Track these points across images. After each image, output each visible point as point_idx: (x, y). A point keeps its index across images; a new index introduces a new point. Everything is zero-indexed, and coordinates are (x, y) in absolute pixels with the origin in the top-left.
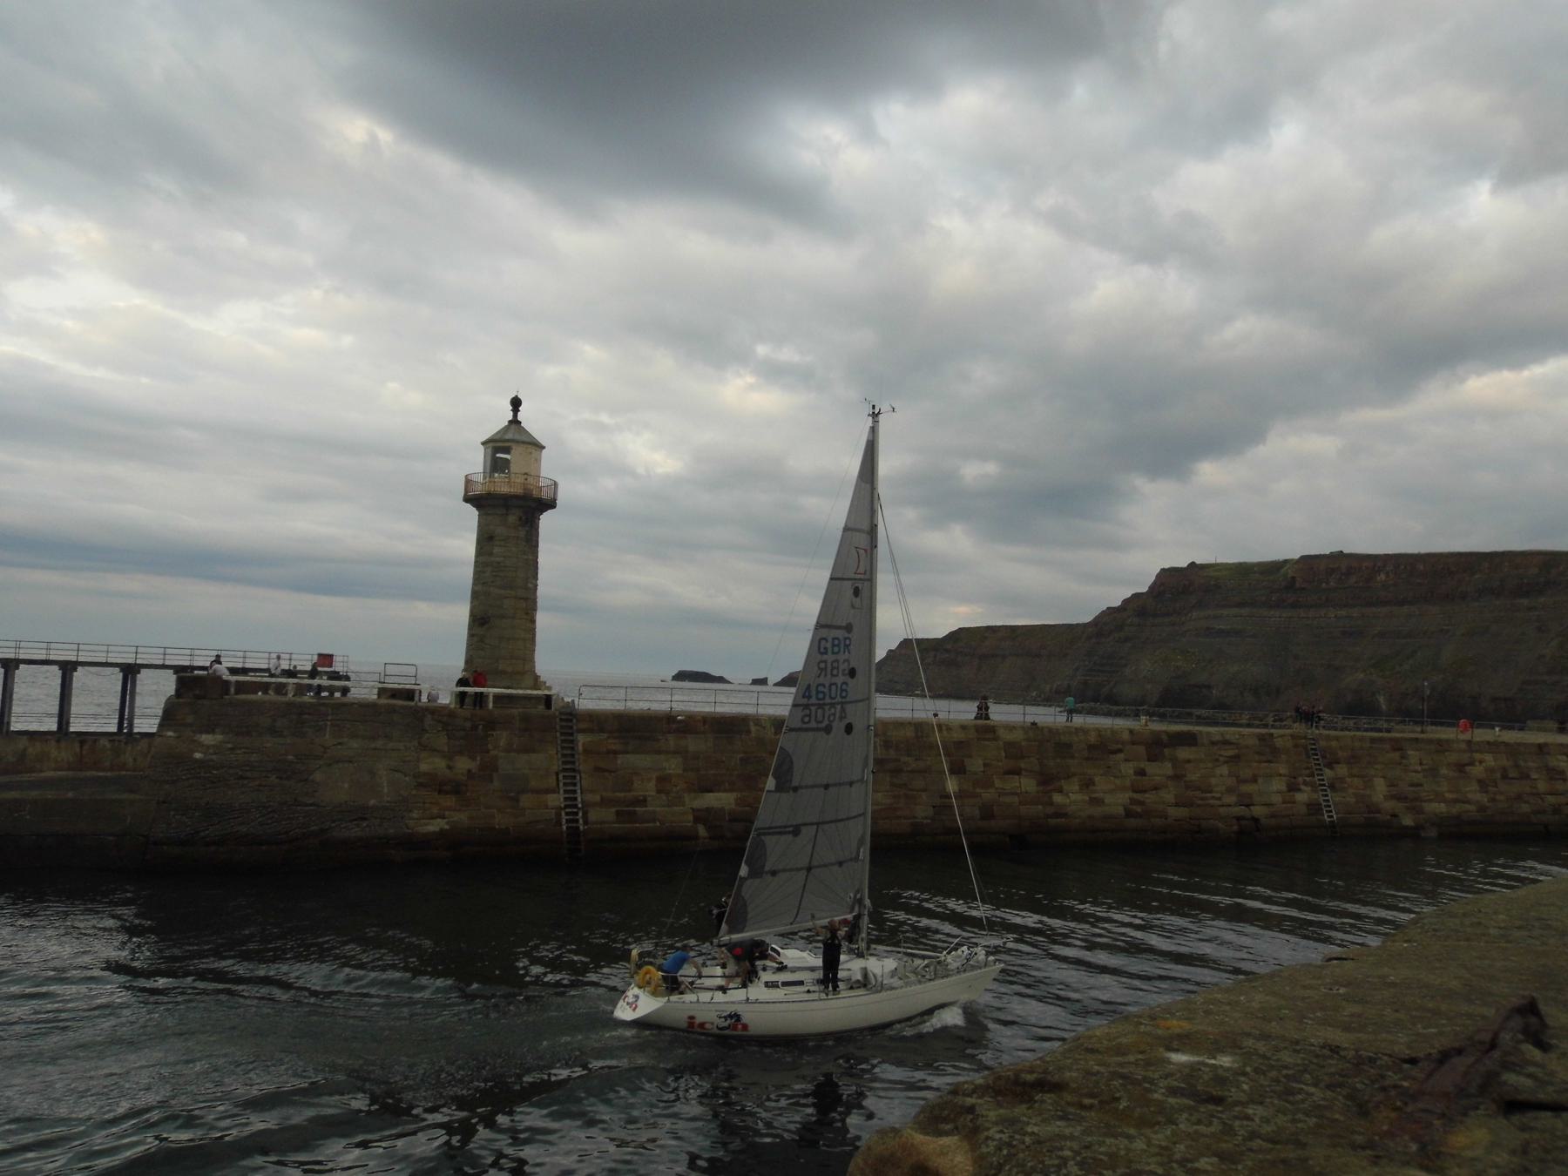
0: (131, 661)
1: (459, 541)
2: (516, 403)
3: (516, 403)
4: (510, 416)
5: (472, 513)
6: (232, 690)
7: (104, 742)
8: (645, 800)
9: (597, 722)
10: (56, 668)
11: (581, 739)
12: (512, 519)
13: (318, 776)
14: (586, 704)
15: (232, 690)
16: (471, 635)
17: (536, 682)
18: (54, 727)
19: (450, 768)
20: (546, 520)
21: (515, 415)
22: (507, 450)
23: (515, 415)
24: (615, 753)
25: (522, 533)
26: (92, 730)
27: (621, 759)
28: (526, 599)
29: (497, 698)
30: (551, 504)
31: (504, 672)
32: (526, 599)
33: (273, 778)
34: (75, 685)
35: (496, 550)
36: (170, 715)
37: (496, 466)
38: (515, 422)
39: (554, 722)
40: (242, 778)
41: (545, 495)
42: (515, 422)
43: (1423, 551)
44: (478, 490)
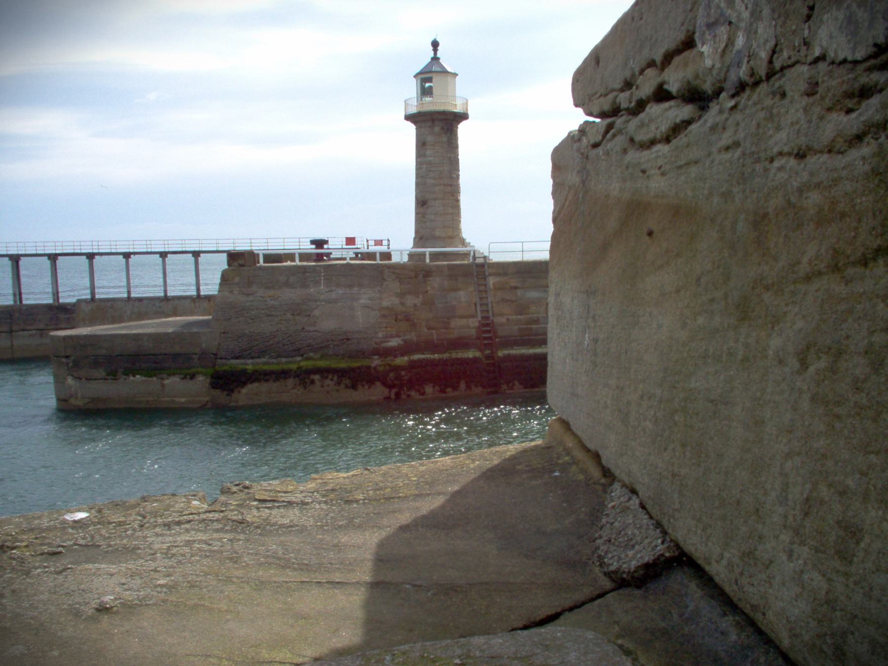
0: (91, 251)
1: (402, 145)
2: (435, 45)
3: (435, 45)
4: (432, 54)
5: (411, 129)
6: (261, 260)
7: (83, 304)
8: (538, 320)
9: (504, 269)
10: (84, 257)
11: (491, 281)
12: (437, 129)
13: (317, 313)
14: (495, 258)
15: (261, 260)
16: (417, 214)
17: (463, 242)
18: (89, 297)
19: (402, 304)
20: (463, 129)
21: (435, 53)
22: (430, 80)
23: (435, 53)
24: (516, 288)
25: (445, 139)
26: (111, 296)
27: (519, 293)
28: (451, 185)
29: (431, 254)
30: (464, 116)
31: (439, 238)
32: (451, 185)
33: (289, 315)
34: (11, 274)
35: (428, 152)
36: (225, 278)
37: (425, 92)
38: (435, 59)
39: (479, 271)
40: (269, 315)
41: (458, 109)
42: (435, 59)
43: (460, 157)
44: (413, 110)
